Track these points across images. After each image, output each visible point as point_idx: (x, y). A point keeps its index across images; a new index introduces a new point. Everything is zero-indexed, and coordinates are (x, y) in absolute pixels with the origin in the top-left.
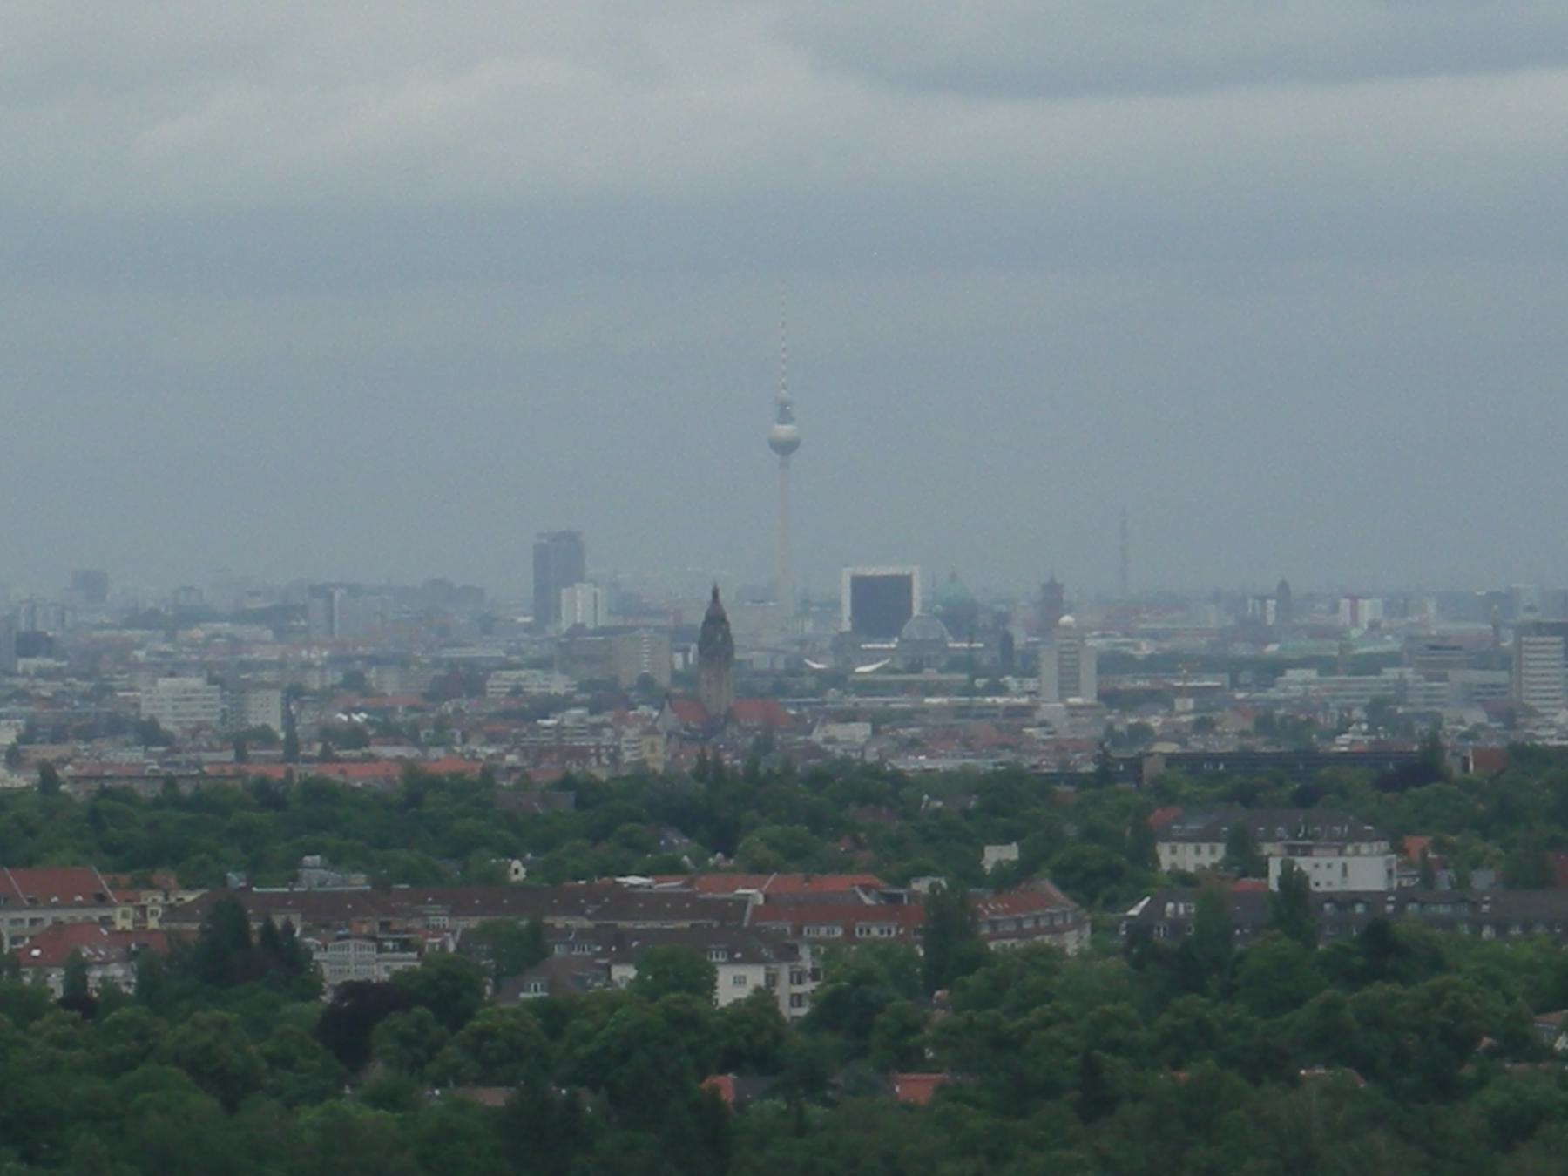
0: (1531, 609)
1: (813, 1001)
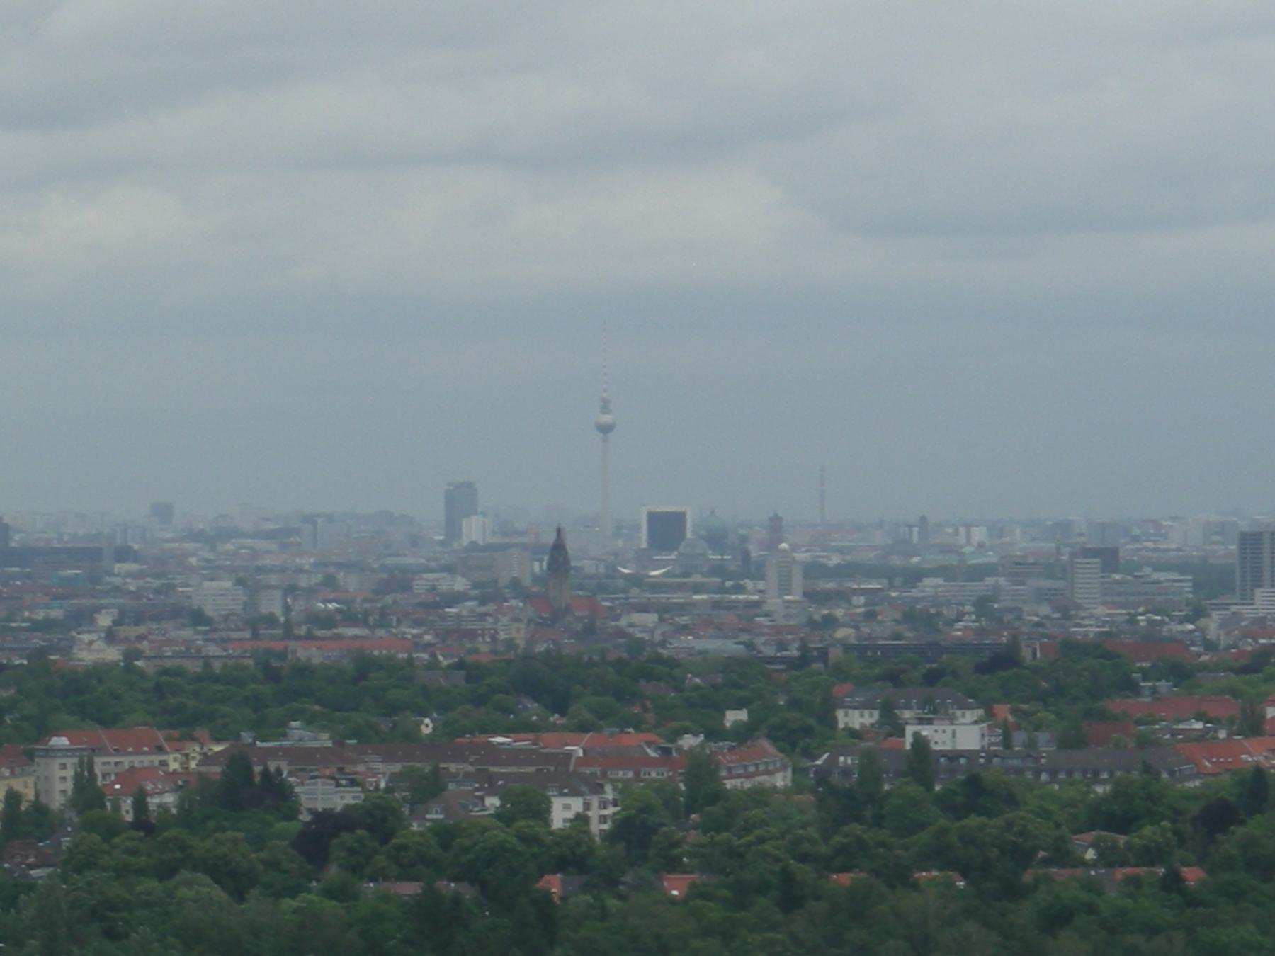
0: (1081, 535)
1: (613, 822)
